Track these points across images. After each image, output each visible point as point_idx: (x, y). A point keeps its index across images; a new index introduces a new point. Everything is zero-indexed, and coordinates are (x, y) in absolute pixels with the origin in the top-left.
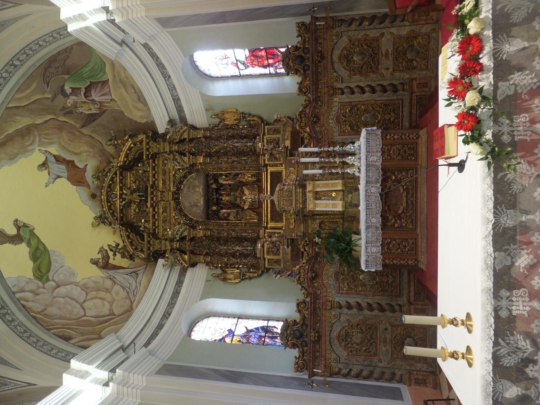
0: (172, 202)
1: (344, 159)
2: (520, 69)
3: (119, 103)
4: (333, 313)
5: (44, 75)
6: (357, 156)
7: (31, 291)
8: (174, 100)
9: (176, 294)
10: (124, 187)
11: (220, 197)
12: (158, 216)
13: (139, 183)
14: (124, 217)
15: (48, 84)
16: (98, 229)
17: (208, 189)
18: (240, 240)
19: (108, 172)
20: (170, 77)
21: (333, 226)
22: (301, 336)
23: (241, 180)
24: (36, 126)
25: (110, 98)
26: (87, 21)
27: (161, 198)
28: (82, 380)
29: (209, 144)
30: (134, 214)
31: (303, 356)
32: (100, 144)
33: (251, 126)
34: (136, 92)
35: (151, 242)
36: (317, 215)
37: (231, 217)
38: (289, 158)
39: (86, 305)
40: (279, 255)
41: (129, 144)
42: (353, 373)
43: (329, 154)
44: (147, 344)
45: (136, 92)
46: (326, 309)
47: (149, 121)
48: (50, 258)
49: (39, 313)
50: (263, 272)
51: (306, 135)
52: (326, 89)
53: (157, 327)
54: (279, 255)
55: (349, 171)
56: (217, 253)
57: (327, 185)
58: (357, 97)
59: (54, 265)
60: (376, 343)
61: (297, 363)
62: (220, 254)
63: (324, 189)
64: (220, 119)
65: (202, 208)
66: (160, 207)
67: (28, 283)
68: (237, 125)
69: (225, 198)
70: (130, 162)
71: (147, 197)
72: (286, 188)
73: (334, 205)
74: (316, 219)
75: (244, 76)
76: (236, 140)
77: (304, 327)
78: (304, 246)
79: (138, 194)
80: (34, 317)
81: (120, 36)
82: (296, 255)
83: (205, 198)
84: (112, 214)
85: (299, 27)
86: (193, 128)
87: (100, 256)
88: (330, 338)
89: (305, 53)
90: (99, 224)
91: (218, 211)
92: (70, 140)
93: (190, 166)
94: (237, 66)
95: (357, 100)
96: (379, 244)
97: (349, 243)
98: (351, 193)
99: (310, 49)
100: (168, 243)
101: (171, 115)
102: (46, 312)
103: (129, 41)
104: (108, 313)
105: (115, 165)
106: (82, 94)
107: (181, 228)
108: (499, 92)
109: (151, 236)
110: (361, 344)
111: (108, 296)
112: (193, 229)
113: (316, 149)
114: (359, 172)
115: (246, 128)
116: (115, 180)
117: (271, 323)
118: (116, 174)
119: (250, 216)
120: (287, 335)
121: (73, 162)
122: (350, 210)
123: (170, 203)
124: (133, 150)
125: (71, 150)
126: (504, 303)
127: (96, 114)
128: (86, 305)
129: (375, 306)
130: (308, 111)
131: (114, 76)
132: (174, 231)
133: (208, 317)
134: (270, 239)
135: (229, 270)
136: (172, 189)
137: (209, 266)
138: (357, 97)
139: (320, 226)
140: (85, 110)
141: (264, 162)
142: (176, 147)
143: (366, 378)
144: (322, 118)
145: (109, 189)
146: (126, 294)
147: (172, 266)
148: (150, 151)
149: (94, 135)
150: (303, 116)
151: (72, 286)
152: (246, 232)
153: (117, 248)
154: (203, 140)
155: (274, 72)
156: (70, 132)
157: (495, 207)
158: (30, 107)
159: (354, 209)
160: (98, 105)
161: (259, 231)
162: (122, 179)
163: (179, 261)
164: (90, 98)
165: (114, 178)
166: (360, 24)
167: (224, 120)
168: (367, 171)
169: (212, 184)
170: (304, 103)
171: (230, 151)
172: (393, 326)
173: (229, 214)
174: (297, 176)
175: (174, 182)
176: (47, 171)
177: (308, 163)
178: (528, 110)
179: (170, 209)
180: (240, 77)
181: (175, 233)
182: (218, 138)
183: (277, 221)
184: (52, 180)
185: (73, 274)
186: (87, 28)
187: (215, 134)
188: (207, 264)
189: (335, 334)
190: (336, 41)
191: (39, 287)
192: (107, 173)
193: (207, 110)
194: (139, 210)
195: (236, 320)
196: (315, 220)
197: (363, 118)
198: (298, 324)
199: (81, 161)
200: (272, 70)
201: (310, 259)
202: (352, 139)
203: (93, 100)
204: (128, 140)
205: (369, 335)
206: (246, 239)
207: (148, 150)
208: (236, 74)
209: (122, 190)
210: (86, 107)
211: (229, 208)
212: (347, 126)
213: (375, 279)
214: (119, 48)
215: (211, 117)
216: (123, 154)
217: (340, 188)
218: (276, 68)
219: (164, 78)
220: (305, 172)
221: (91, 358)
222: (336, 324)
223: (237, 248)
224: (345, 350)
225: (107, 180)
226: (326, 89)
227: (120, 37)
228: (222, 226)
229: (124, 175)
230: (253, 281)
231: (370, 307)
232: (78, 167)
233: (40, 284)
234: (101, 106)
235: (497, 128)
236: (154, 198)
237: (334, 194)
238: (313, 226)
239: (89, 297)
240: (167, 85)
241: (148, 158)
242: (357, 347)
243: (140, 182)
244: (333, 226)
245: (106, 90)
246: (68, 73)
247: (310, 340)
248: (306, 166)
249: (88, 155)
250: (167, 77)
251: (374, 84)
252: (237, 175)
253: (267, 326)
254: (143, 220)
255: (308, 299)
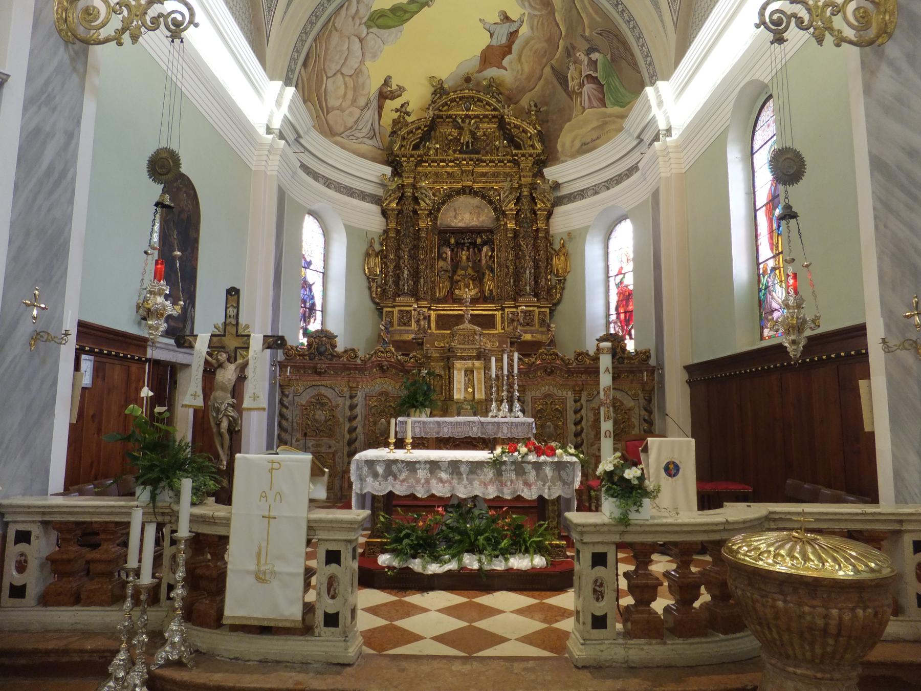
0: (460, 186)
1: (505, 401)
2: (537, 475)
3: (581, 117)
4: (345, 389)
5: (610, 32)
6: (508, 414)
7: (357, 11)
8: (582, 190)
9: (350, 192)
10: (478, 120)
11: (465, 248)
12: (443, 167)
13: (483, 140)
14: (442, 120)
15: (600, 34)
16: (427, 83)
17: (476, 232)
18: (415, 275)
19: (497, 99)
20: (608, 188)
21: (438, 389)
22: (321, 354)
23: (487, 276)
24: (552, 12)
25: (586, 106)
26: (657, 109)
27: (466, 171)
28: (274, 102)
29: (529, 236)
30: (445, 132)
31: (300, 355)
32: (532, 87)
33: (549, 291)
34: (593, 141)
35: (413, 159)
36: (449, 371)
37: (441, 263)
38: (509, 340)
39: (339, 76)
40: (399, 325)
41: (531, 130)
42: (284, 410)
43: (511, 386)
44: (304, 167)
45: (593, 141)
46: (349, 381)
47: (560, 155)
48: (394, 27)
49: (334, 24)
50: (378, 304)
51: (533, 360)
52: (580, 383)
53: (316, 173)
54: (399, 325)
55: (494, 405)
56: (399, 245)
57: (479, 383)
58: (571, 417)
59: (386, 32)
60: (316, 436)
61: (292, 348)
62: (398, 248)
63: (475, 380)
64: (559, 250)
65: (453, 224)
66: (455, 169)
67: (367, 5)
68: (551, 272)
69: (464, 255)
70: (510, 130)
71: (466, 153)
72: (477, 338)
73: (459, 390)
74: (444, 370)
75: (608, 281)
76: (533, 271)
77: (330, 357)
78: (415, 357)
79: (470, 141)
80: (330, 19)
81: (647, 137)
82: (403, 347)
83: (464, 228)
84: (446, 104)
85: (645, 352)
86: (550, 214)
87: (394, 87)
88: (319, 386)
89: (618, 359)
90: (433, 86)
91: (449, 245)
92: (536, 51)
93: (503, 211)
94: (620, 273)
95: (568, 416)
96: (423, 435)
97: (423, 406)
98: (472, 409)
99: (622, 365)
100: (411, 181)
101: (565, 185)
102: (334, 32)
103: (643, 147)
104: (329, 106)
105: (506, 111)
106: (591, 73)
107: (429, 199)
108: (526, 465)
109: (419, 159)
110: (314, 419)
111: (348, 102)
112: (428, 214)
113: (516, 371)
114: (492, 417)
115: (547, 284)
116: (487, 107)
117: (319, 315)
118: (495, 109)
119: (443, 287)
120: (321, 338)
121: (510, 52)
122: (455, 407)
123: (459, 183)
124: (524, 134)
125: (525, 51)
126: (423, 466)
127: (568, 86)
128: (339, 76)
129: (354, 435)
130: (558, 362)
131: (610, 116)
132: (426, 190)
133: (324, 235)
134: (422, 318)
135: (378, 260)
136: (476, 185)
137: (384, 234)
138: (571, 417)
139: (438, 375)
140: (571, 73)
141: (506, 307)
142: (526, 193)
143: (280, 425)
144: (550, 378)
145: (476, 100)
146: (349, 125)
147: (383, 185)
148: (522, 158)
149: (542, 81)
150: (553, 356)
151: (360, 58)
152: (425, 283)
153: (404, 113)
154: (534, 228)
155: (611, 320)
156: (546, 52)
157: (470, 462)
158: (574, 11)
159: (455, 412)
160: (578, 89)
161: (426, 300)
162: (488, 117)
163: (390, 195)
164: (585, 82)
165: (490, 106)
166: (645, 420)
167: (558, 255)
168: (493, 423)
169: (481, 237)
170: (566, 358)
171: (520, 263)
172: (334, 454)
173: (445, 260)
174: (489, 350)
175: (484, 188)
176: (499, 21)
177: (502, 363)
178: (517, 478)
179: (452, 183)
180: (607, 277)
181: (424, 191)
182: (535, 248)
183: (437, 322)
184: (487, 27)
185: (374, 56)
186: (650, 107)
187: (541, 244)
188: (386, 232)
189: (323, 392)
190: (630, 394)
191: (361, 19)
192: (496, 98)
193: (569, 234)
194: (451, 140)
195: (322, 270)
196: (444, 369)
197: (549, 423)
198: (333, 349)
199: (511, 63)
200: (613, 317)
201: (402, 364)
202: (528, 412)
203: (583, 85)
204: (535, 129)
205: (324, 429)
206: (416, 283)
207: (523, 155)
208: (610, 272)
209: (475, 117)
210: (576, 75)
211: (452, 260)
212: (541, 406)
213: (382, 435)
214: (636, 134)
215: (562, 239)
216: (518, 122)
217: (477, 396)
218: (615, 323)
219: (607, 181)
220: (493, 359)
221: (294, 109)
222: (334, 393)
223: (406, 272)
224: (307, 402)
225: (488, 98)
226: (580, 383)
227: (647, 137)
228: (431, 251)
229: (493, 120)
230: (367, 292)
231: (352, 430)
232: (503, 59)
233: (364, 20)
234: (577, 94)
235: (509, 463)
236: (465, 162)
237: (470, 390)
238: (438, 367)
239: (347, 79)
240: (599, 184)
241: (513, 155)
242: (311, 415)
243: (485, 141)
244: (438, 389)
245: (595, 103)
246: (613, 60)
247: (317, 364)
248: (499, 360)
249: (518, 72)
250: (608, 184)
251: (584, 435)
252: (492, 271)
253: (315, 310)
254: (438, 146)
255: (359, 361)
